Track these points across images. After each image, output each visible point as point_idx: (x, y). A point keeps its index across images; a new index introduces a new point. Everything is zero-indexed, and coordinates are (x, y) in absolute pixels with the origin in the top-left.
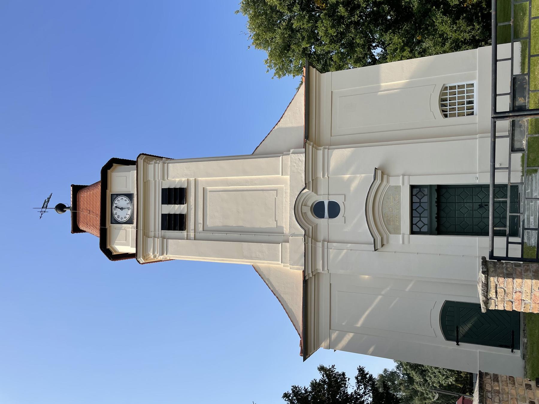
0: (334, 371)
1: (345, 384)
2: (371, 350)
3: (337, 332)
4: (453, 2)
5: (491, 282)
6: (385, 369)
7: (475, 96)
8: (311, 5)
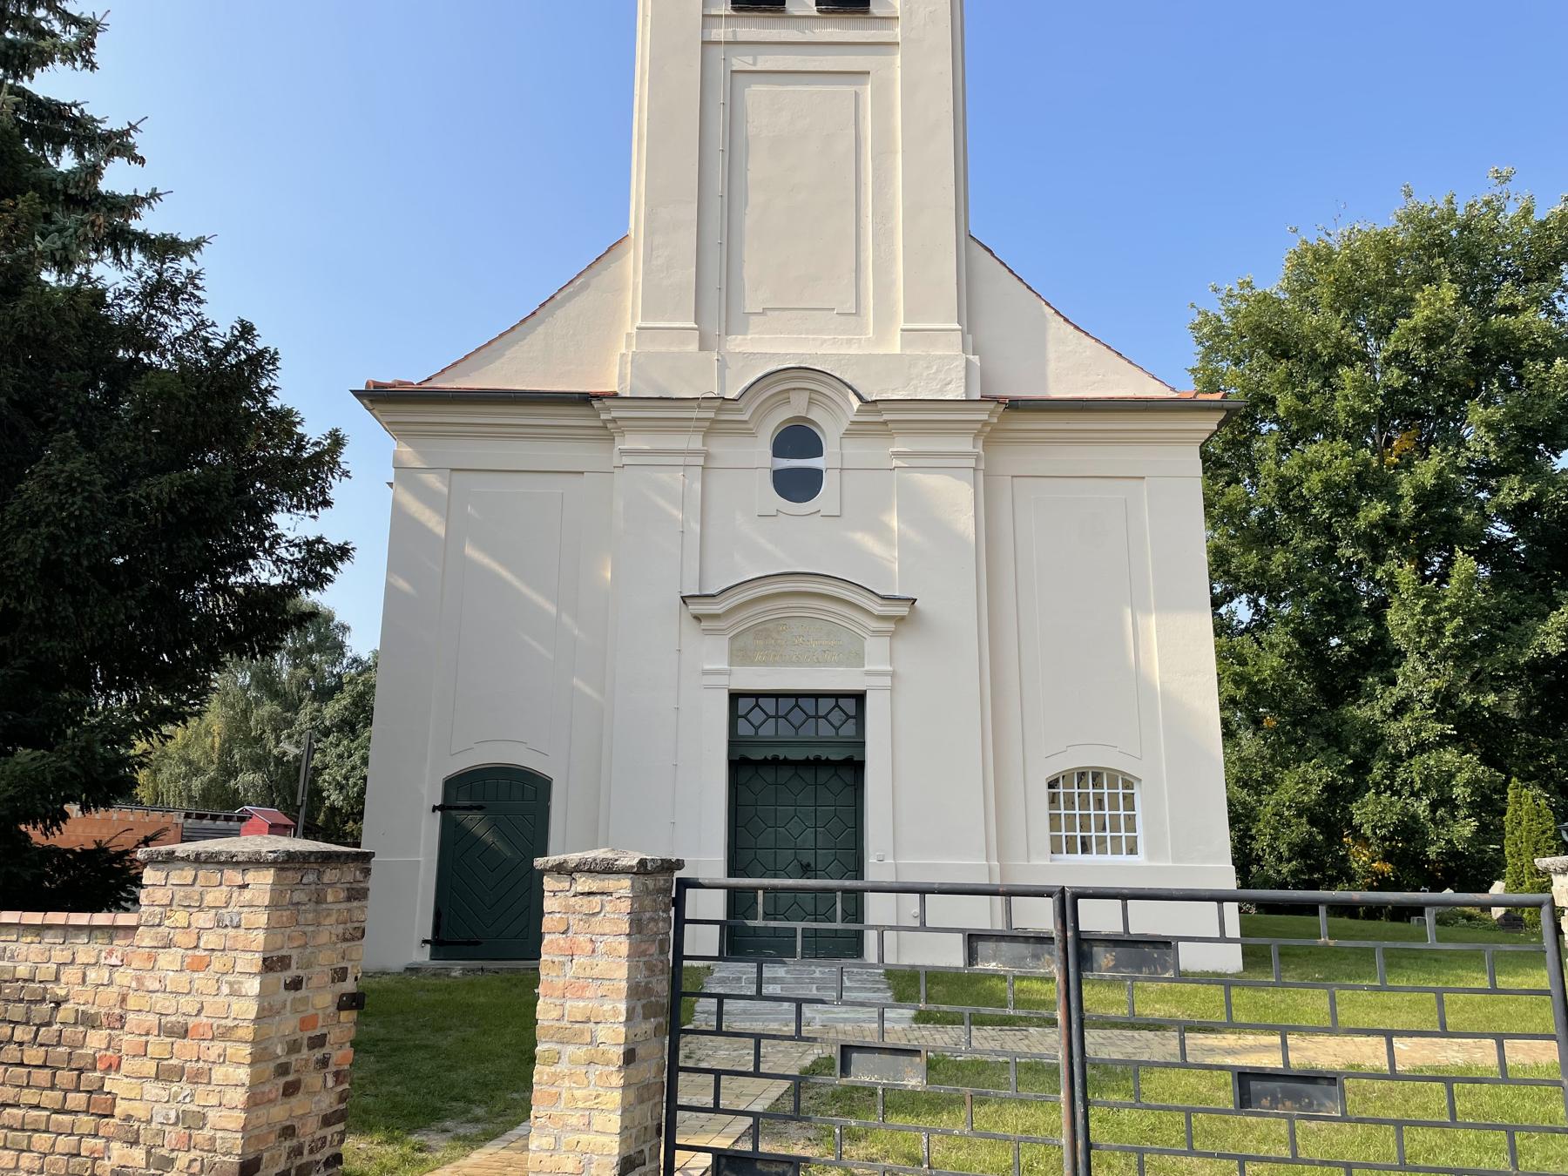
0: (334, 478)
1: (299, 507)
2: (402, 584)
3: (445, 490)
4: (1359, 809)
5: (619, 880)
6: (349, 629)
7: (1102, 857)
8: (1397, 422)
